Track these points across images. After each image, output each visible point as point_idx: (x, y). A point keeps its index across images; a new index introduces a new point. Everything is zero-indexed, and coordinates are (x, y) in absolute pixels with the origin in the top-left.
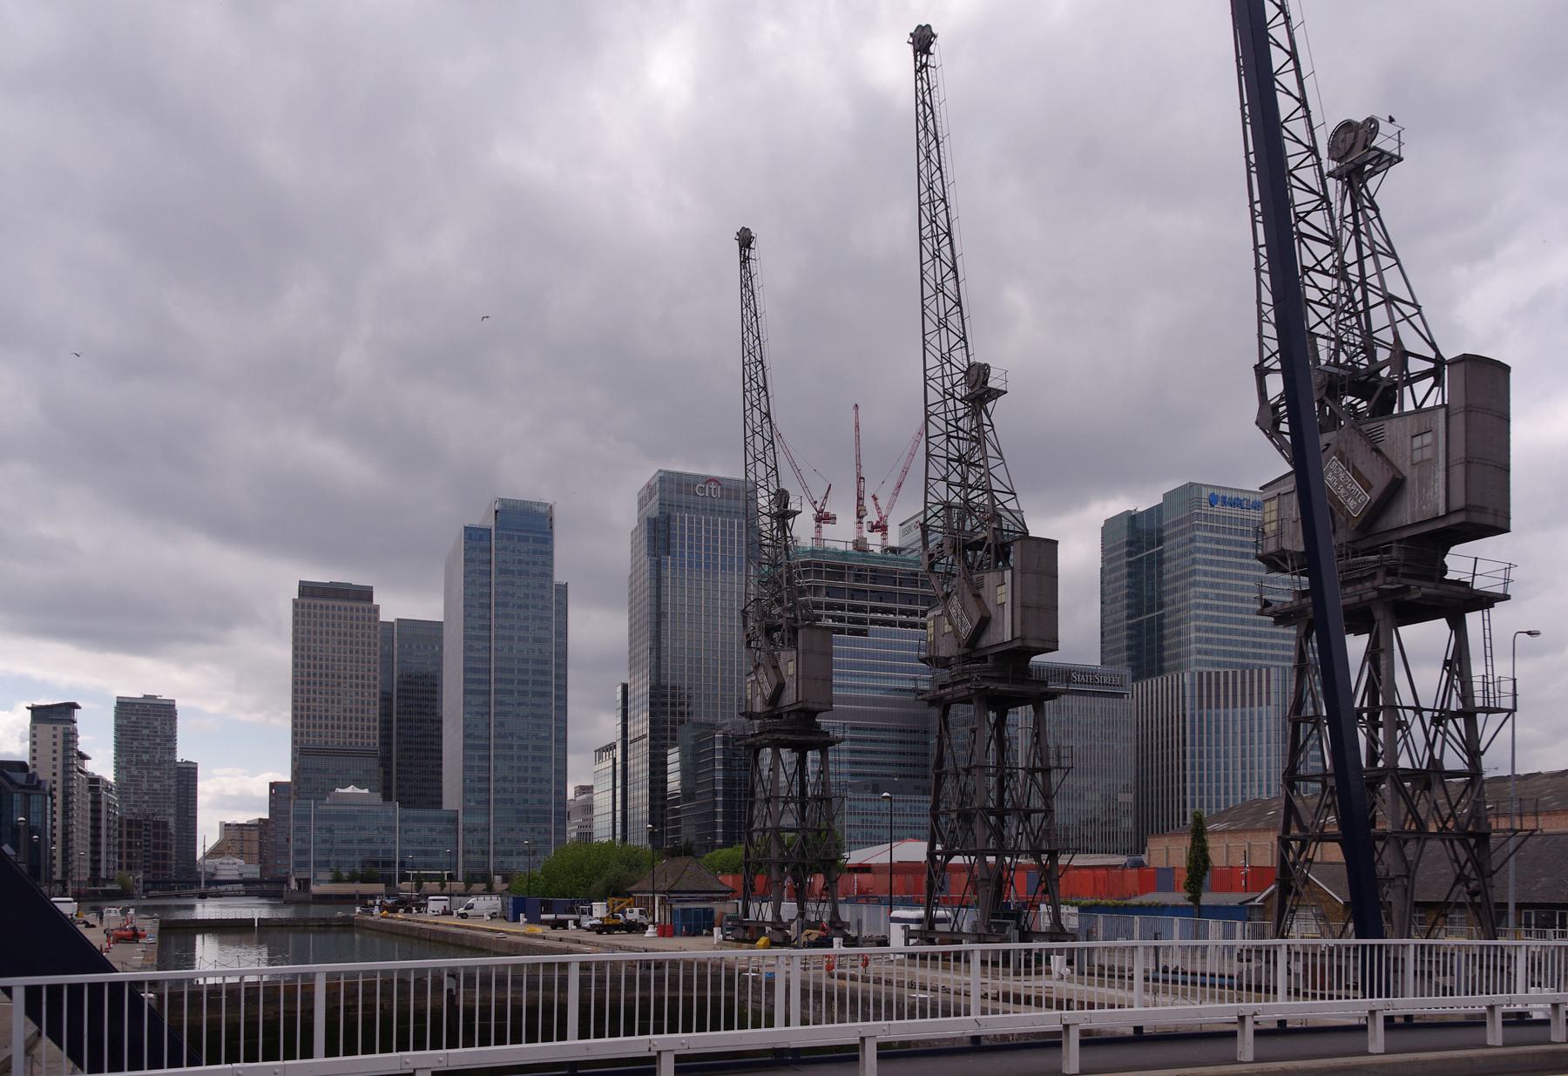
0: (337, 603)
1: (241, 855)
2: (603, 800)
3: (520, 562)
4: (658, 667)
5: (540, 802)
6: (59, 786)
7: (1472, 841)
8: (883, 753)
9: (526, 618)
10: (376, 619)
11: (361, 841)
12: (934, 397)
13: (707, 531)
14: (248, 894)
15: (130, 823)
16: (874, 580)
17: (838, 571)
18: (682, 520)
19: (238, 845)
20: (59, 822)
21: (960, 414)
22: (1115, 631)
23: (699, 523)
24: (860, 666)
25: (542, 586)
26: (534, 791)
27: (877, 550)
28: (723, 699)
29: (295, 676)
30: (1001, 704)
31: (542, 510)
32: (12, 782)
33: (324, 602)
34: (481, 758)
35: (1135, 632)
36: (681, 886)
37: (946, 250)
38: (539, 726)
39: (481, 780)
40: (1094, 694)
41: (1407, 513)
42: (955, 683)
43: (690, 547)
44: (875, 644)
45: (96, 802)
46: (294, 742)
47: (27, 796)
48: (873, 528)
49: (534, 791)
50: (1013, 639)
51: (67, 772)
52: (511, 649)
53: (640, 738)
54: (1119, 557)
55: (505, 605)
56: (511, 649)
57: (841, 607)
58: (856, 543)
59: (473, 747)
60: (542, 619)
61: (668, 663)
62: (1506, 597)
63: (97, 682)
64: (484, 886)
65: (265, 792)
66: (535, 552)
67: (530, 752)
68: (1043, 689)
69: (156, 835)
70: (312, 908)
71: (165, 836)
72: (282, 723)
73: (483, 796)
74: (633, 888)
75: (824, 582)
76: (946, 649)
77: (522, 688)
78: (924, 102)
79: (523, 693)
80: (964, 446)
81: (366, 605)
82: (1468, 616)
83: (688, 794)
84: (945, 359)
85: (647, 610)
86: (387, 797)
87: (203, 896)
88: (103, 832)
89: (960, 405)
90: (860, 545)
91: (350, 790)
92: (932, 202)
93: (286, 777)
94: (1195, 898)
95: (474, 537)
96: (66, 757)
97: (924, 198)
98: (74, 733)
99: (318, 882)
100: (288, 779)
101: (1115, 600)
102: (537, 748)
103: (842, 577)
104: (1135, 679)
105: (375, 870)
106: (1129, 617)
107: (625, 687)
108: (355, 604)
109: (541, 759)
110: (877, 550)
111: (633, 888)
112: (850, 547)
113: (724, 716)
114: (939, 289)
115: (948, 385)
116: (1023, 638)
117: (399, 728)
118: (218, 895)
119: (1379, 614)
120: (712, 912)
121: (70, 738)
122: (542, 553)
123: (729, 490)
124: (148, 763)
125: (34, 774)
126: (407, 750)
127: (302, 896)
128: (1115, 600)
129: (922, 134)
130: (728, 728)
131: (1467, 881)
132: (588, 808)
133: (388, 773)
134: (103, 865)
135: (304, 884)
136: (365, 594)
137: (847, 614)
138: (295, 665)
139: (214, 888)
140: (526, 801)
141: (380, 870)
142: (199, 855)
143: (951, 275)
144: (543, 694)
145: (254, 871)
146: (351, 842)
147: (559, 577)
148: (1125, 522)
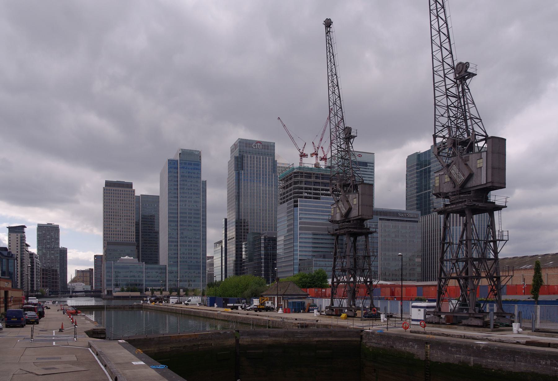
0: (120, 189)
1: (83, 282)
2: (217, 262)
3: (189, 173)
4: (239, 209)
5: (197, 262)
6: (19, 256)
7: (495, 279)
8: (320, 247)
9: (191, 194)
10: (134, 195)
11: (131, 277)
12: (332, 127)
13: (257, 161)
14: (86, 296)
15: (43, 270)
16: (323, 178)
17: (309, 175)
18: (248, 157)
19: (82, 278)
20: (19, 270)
21: (342, 143)
22: (411, 198)
23: (254, 158)
24: (317, 211)
25: (197, 182)
26: (194, 258)
27: (323, 167)
28: (263, 224)
29: (104, 216)
30: (355, 235)
31: (197, 153)
32: (2, 255)
33: (115, 188)
34: (175, 246)
35: (419, 198)
36: (289, 292)
37: (337, 91)
38: (196, 234)
39: (175, 254)
40: (407, 221)
41: (473, 183)
42: (340, 229)
43: (251, 167)
44: (323, 203)
45: (32, 263)
46: (104, 240)
47: (8, 260)
48: (322, 159)
49: (194, 258)
50: (487, 183)
51: (22, 251)
52: (185, 205)
53: (232, 239)
54: (413, 170)
55: (183, 189)
56: (185, 205)
57: (310, 189)
58: (315, 165)
59: (172, 242)
60: (197, 194)
61: (242, 210)
62: (506, 207)
63: (32, 218)
64: (176, 293)
65: (92, 260)
66: (194, 169)
67: (193, 244)
68: (368, 231)
69: (53, 275)
70: (113, 301)
71: (56, 275)
72: (99, 233)
73: (176, 260)
74: (264, 293)
75: (304, 179)
76: (338, 218)
77: (190, 219)
78: (329, 43)
79: (190, 222)
80: (343, 153)
81: (130, 189)
82: (495, 212)
83: (250, 259)
84: (337, 126)
85: (234, 191)
86: (139, 260)
87: (71, 297)
88: (35, 273)
89: (341, 140)
90: (317, 165)
91: (126, 257)
92: (332, 75)
93: (101, 252)
94: (536, 297)
95: (172, 164)
96: (21, 246)
97: (330, 74)
98: (24, 237)
99: (116, 292)
100: (102, 254)
101: (411, 186)
102: (196, 242)
103: (310, 177)
104: (422, 215)
105: (136, 287)
106: (417, 192)
107: (226, 220)
108: (126, 189)
109: (197, 246)
110: (323, 167)
111: (264, 293)
112: (313, 166)
113: (263, 230)
114: (335, 103)
115: (338, 134)
116: (492, 182)
117: (142, 235)
118: (76, 296)
119: (467, 212)
120: (304, 303)
121: (23, 238)
122: (197, 169)
123: (265, 146)
124: (49, 248)
125: (10, 252)
126: (145, 243)
127: (109, 297)
128: (411, 186)
129: (328, 53)
130: (266, 234)
131: (494, 291)
132: (212, 265)
133: (138, 252)
134: (35, 285)
135: (110, 292)
136: (130, 185)
137: (312, 191)
138: (104, 212)
139: (74, 294)
140: (191, 262)
141: (138, 287)
142: (68, 282)
143: (338, 99)
144: (197, 222)
145: (89, 288)
146: (127, 277)
147: (203, 178)
148: (416, 157)
